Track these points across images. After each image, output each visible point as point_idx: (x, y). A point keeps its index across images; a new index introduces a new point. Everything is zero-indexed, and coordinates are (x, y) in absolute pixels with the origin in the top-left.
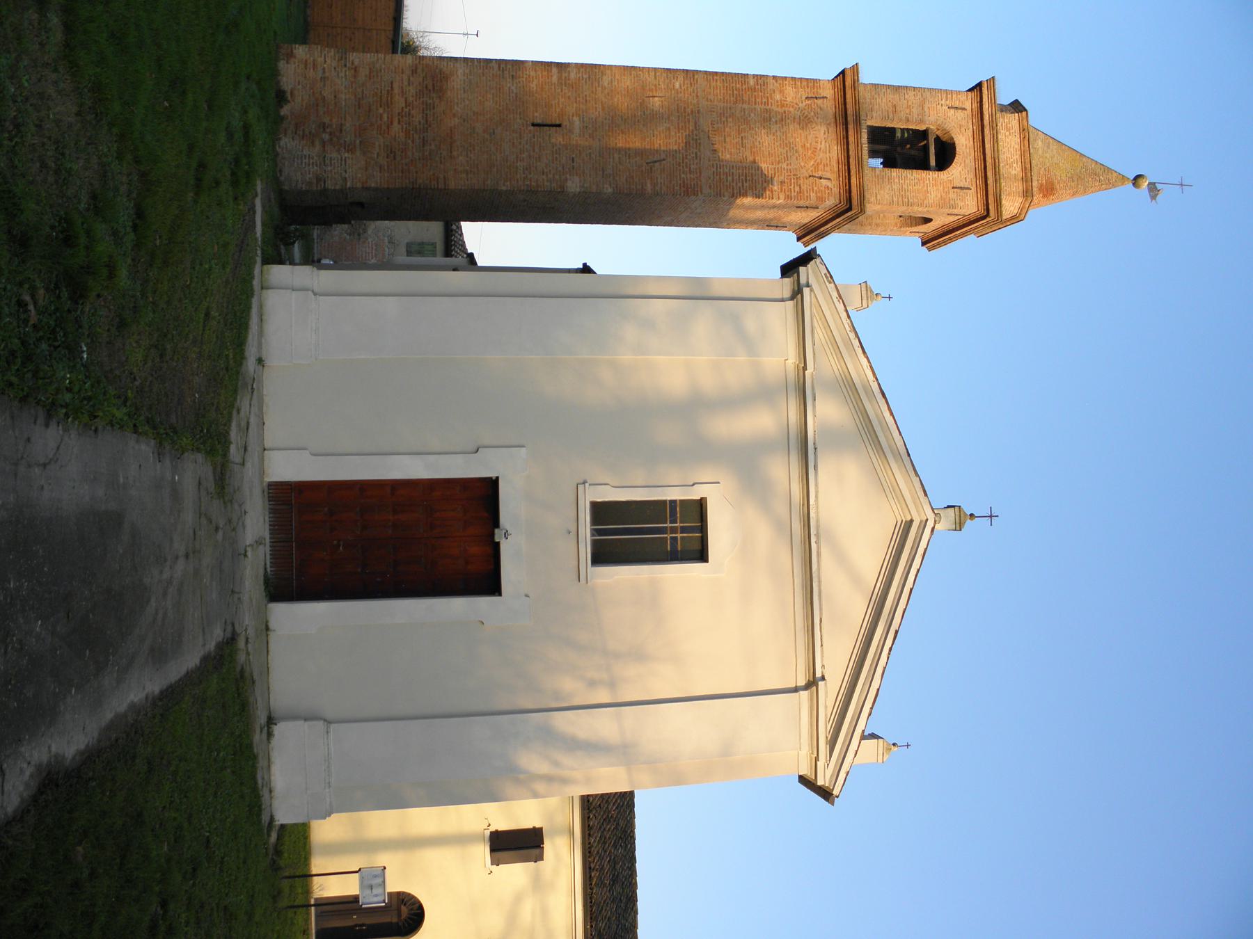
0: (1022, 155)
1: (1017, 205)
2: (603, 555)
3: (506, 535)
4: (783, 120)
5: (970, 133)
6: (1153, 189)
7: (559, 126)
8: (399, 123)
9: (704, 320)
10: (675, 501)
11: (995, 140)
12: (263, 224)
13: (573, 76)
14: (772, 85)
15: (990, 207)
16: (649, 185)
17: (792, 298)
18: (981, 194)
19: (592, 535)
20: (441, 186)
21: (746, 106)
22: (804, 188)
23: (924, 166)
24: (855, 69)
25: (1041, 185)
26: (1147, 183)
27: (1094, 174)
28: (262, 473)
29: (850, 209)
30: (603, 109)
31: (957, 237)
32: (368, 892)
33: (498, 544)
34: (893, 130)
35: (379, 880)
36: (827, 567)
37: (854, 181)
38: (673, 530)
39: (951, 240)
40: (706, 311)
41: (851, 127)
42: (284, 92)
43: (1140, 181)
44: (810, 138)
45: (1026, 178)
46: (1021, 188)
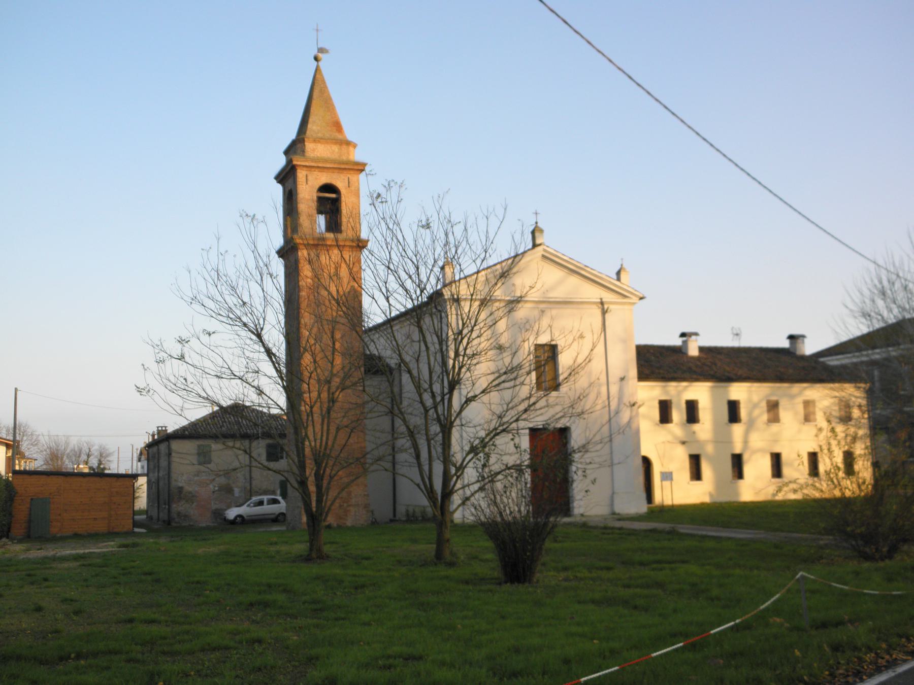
0: (327, 143)
5: (319, 174)
6: (321, 50)
18: (352, 172)
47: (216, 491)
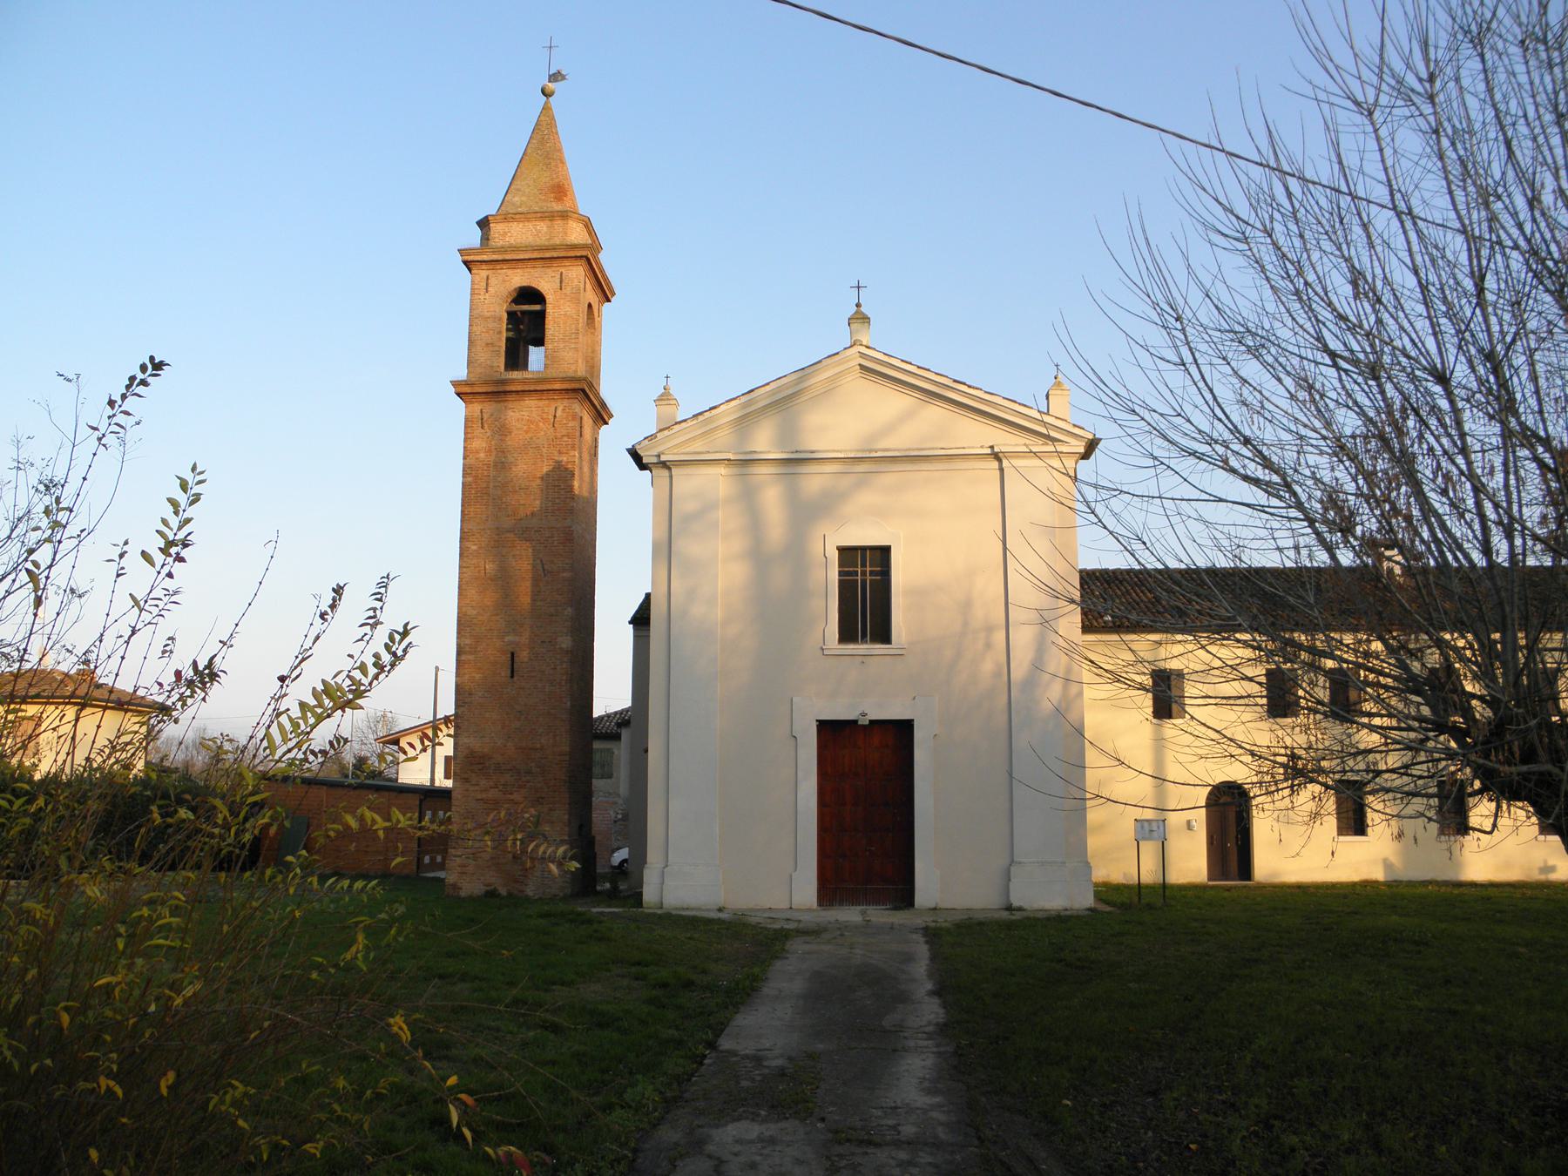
1: (575, 225)
2: (882, 633)
3: (864, 715)
4: (502, 451)
5: (510, 272)
6: (556, 77)
7: (513, 654)
8: (511, 794)
9: (688, 547)
10: (840, 572)
11: (515, 249)
12: (609, 906)
13: (468, 641)
14: (471, 461)
15: (579, 255)
16: (565, 575)
17: (669, 469)
18: (567, 263)
19: (866, 642)
20: (567, 758)
21: (491, 485)
22: (564, 432)
23: (541, 317)
24: (455, 384)
25: (555, 198)
26: (550, 84)
27: (543, 142)
28: (809, 910)
29: (583, 391)
30: (497, 615)
31: (604, 275)
32: (1155, 834)
33: (871, 722)
34: (508, 339)
35: (1146, 824)
36: (896, 442)
37: (557, 386)
38: (864, 573)
39: (606, 279)
40: (680, 545)
41: (508, 388)
42: (487, 892)
43: (547, 91)
44: (519, 426)
45: (550, 216)
46: (559, 222)
47: (619, 820)
